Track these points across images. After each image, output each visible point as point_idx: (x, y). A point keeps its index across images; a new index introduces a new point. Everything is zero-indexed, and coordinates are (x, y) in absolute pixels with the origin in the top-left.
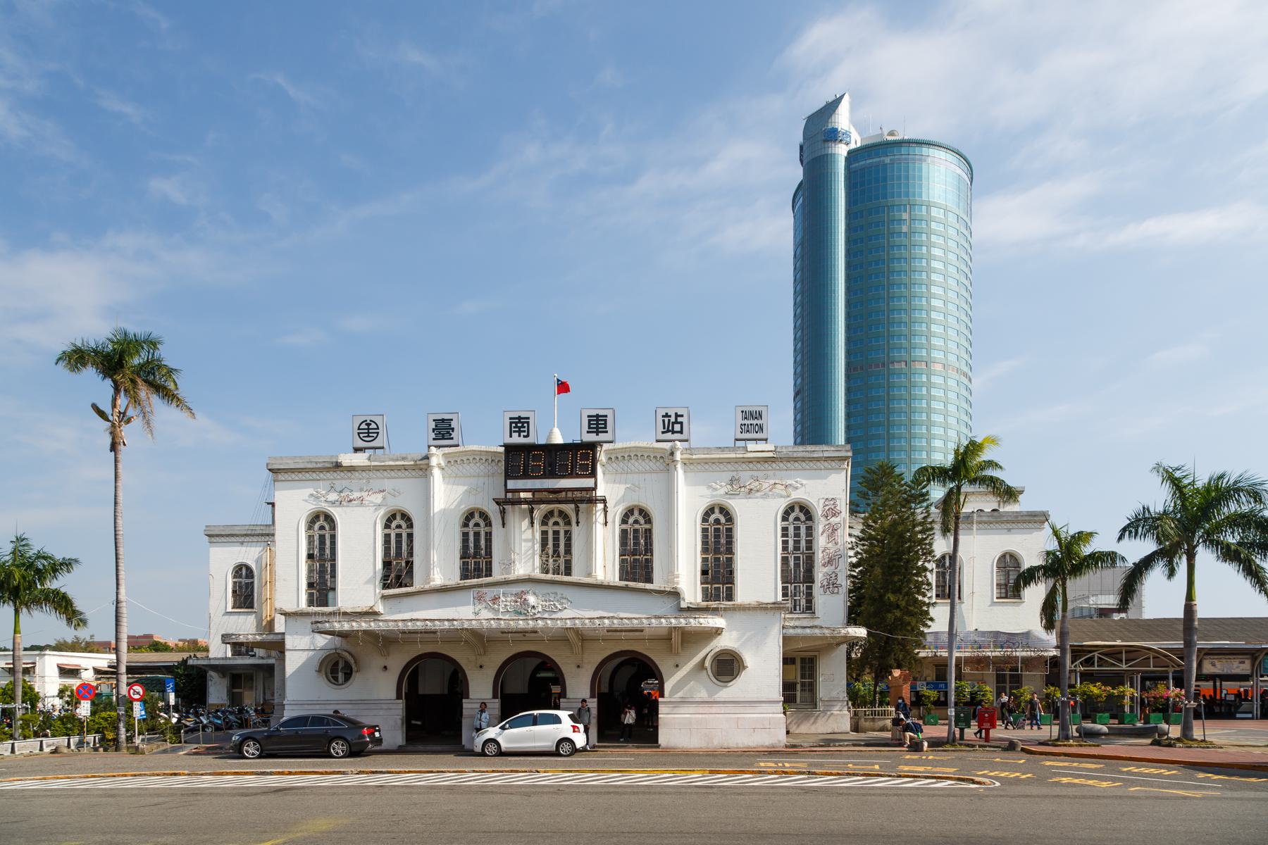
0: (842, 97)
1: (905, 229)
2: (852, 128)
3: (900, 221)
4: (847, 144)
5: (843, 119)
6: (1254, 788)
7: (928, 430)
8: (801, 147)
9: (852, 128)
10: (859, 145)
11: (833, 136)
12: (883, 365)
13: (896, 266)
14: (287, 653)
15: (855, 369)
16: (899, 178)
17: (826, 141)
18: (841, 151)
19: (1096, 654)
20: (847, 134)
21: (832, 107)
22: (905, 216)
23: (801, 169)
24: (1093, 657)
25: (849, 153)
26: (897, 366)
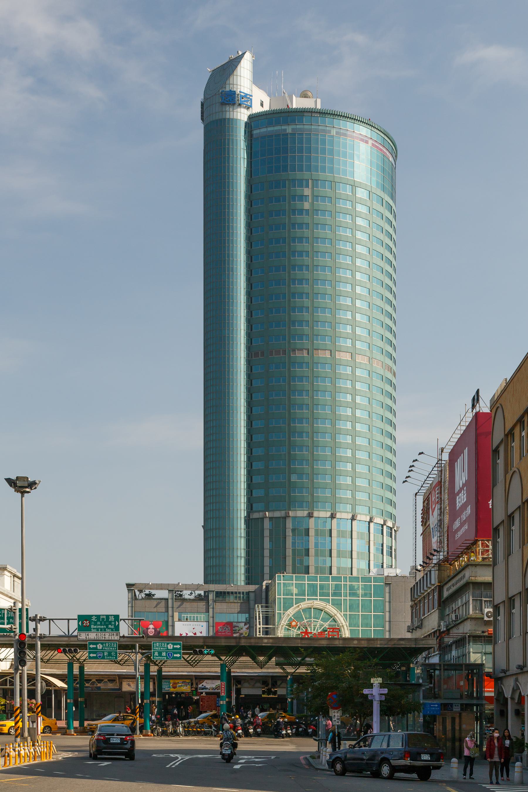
0: (240, 58)
1: (307, 206)
2: (254, 94)
3: (302, 198)
4: (248, 108)
5: (244, 80)
6: (147, 747)
7: (334, 425)
8: (202, 105)
9: (254, 94)
10: (266, 108)
11: (231, 99)
12: (284, 352)
13: (320, 232)
14: (265, 550)
15: (256, 355)
16: (301, 150)
17: (223, 104)
18: (242, 115)
19: (8, 678)
20: (248, 97)
21: (231, 66)
22: (307, 192)
23: (202, 126)
24: (6, 679)
25: (251, 117)
26: (298, 354)
